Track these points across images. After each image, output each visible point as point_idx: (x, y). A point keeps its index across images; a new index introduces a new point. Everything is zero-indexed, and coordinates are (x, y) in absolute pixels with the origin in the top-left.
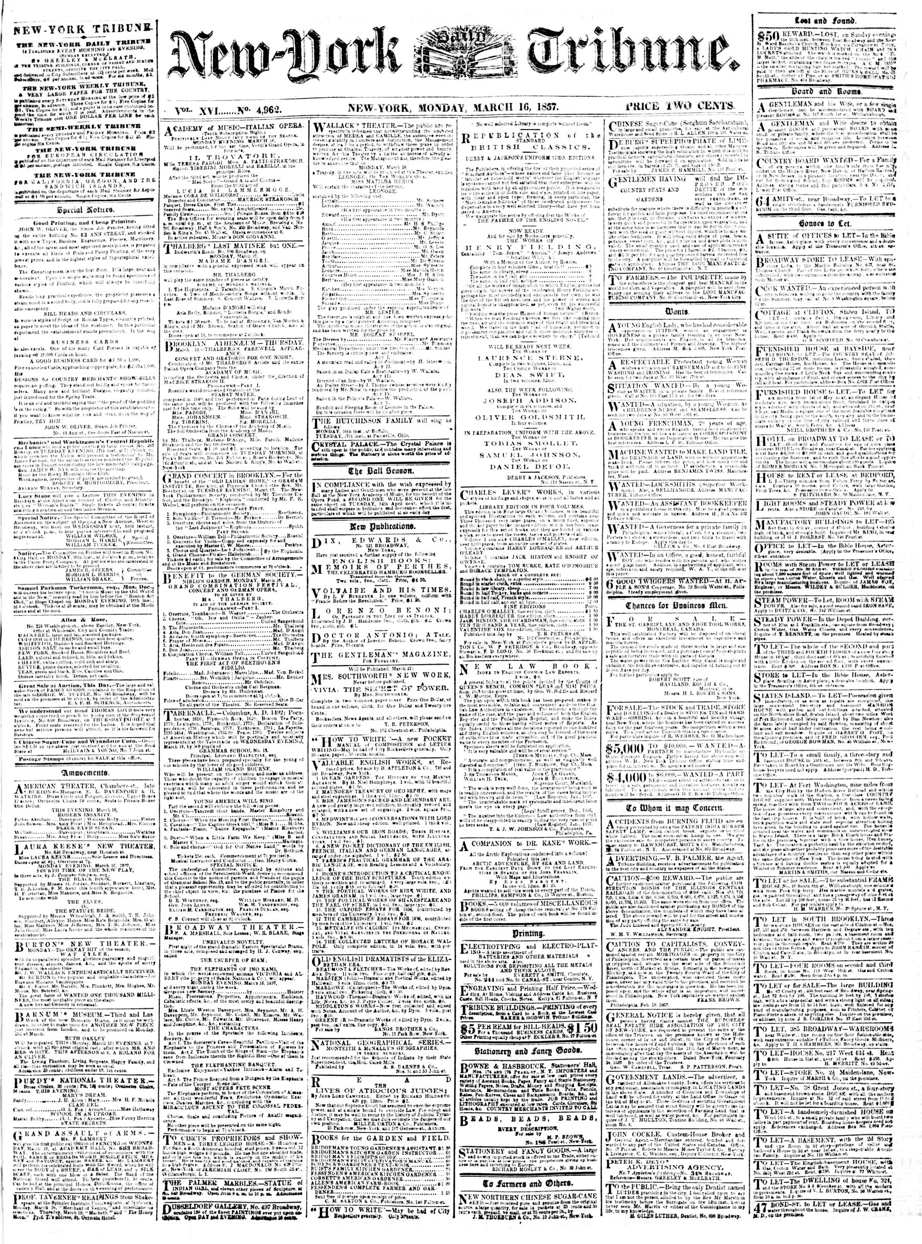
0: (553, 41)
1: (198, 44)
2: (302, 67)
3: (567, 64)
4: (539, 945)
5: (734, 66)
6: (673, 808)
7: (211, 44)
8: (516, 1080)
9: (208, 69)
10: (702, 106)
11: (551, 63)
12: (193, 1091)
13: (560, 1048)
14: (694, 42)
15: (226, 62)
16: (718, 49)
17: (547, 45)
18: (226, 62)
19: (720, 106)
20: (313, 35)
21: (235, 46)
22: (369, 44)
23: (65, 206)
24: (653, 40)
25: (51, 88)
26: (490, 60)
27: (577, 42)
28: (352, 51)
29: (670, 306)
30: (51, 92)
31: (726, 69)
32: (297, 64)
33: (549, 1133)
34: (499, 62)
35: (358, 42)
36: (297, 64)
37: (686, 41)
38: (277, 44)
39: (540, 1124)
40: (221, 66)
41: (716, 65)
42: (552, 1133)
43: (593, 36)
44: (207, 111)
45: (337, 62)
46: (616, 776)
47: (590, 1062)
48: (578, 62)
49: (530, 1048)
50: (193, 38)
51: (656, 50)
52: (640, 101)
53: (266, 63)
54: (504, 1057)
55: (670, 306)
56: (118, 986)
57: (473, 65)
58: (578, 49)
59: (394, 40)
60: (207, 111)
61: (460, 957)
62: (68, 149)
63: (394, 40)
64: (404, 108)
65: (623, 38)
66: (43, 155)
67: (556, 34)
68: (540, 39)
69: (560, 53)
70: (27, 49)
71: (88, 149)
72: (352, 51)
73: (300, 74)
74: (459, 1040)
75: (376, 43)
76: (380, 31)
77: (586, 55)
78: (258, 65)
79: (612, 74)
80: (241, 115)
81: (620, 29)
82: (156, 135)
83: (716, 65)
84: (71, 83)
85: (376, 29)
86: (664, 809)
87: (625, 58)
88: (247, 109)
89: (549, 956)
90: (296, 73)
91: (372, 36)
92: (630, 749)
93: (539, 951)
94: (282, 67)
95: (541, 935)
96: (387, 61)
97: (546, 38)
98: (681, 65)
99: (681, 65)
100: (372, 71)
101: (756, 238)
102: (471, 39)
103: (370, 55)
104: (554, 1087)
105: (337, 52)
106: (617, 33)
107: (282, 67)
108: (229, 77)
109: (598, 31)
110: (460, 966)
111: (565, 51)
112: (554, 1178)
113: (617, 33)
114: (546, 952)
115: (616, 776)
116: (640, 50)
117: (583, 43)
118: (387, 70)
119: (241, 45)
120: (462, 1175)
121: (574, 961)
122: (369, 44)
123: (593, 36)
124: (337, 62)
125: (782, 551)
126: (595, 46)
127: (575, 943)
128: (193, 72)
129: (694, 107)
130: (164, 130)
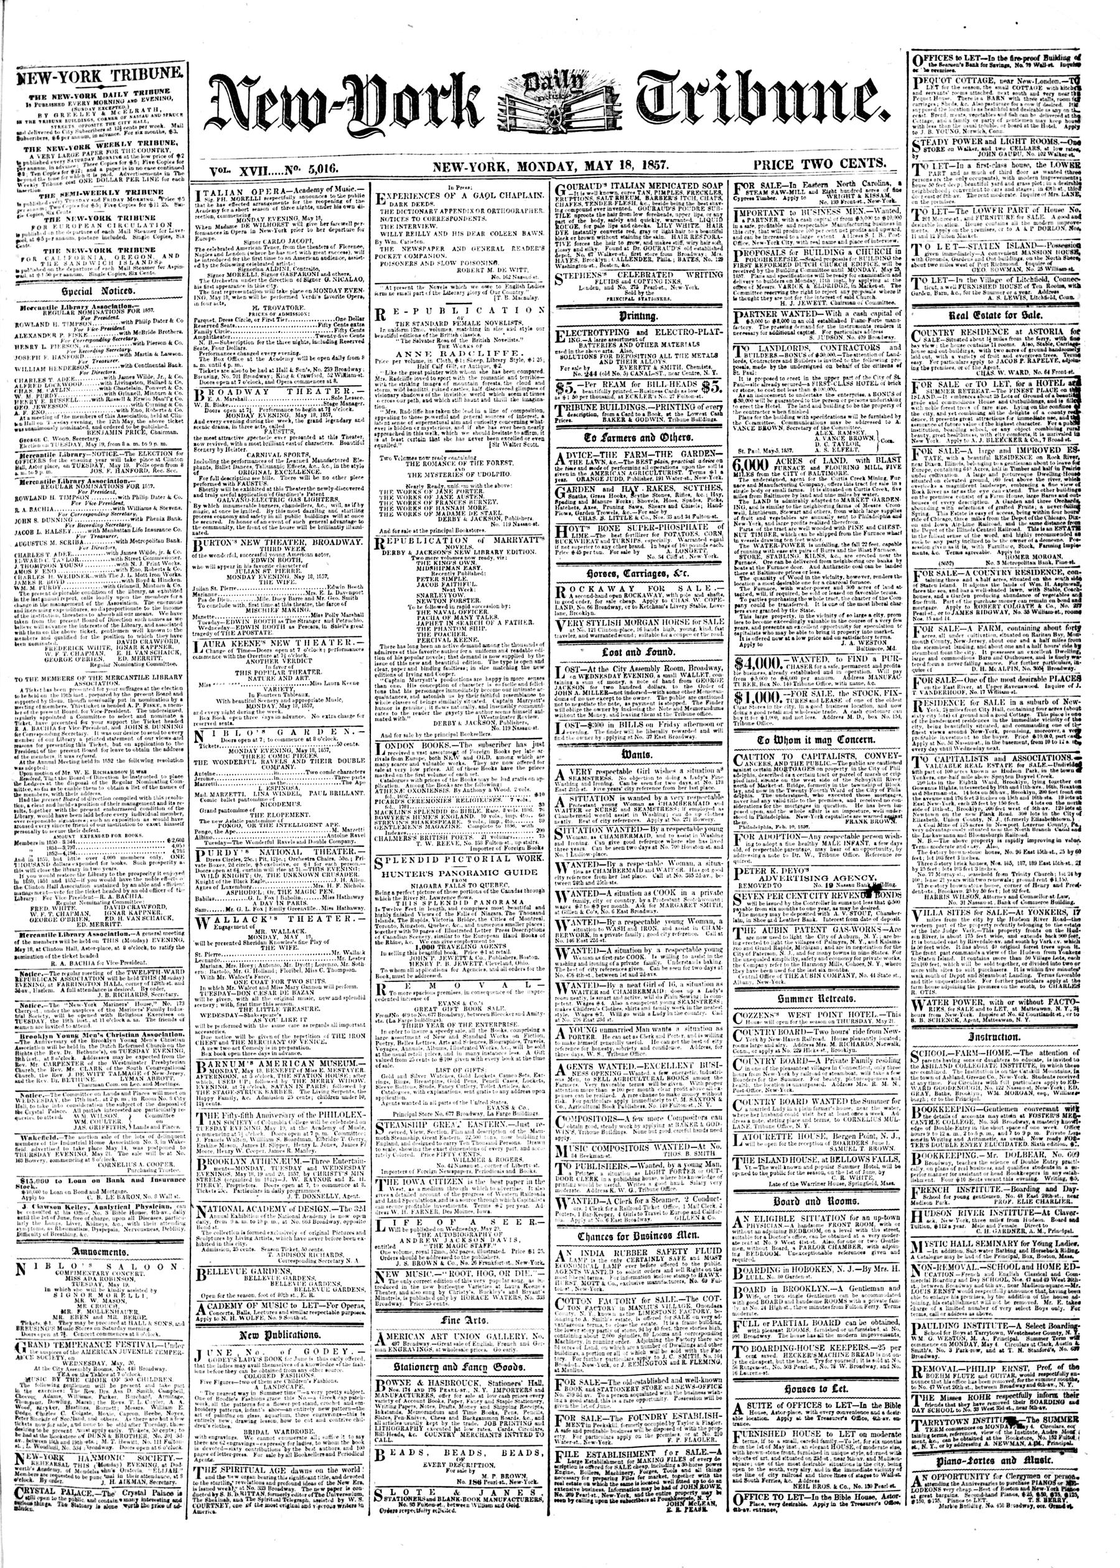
0: (667, 86)
1: (242, 91)
2: (364, 119)
4: (652, 330)
5: (885, 115)
6: (813, 740)
7: (258, 90)
9: (253, 121)
10: (845, 163)
11: (665, 112)
15: (274, 113)
16: (866, 95)
17: (660, 91)
18: (274, 113)
19: (868, 163)
20: (379, 82)
21: (286, 94)
22: (445, 93)
23: (71, 286)
24: (787, 84)
25: (61, 148)
26: (592, 109)
27: (696, 88)
28: (424, 101)
30: (62, 153)
31: (876, 120)
32: (358, 116)
34: (600, 112)
35: (431, 89)
36: (358, 116)
38: (336, 92)
40: (269, 117)
41: (866, 117)
43: (715, 81)
44: (249, 171)
46: (745, 662)
48: (697, 113)
50: (236, 83)
51: (790, 96)
52: (770, 157)
53: (322, 119)
56: (111, 761)
57: (569, 116)
58: (697, 98)
59: (475, 89)
60: (249, 171)
61: (555, 346)
62: (80, 218)
63: (475, 89)
66: (50, 225)
67: (671, 78)
68: (653, 83)
69: (676, 101)
70: (41, 101)
71: (102, 219)
72: (424, 101)
73: (362, 127)
76: (458, 79)
77: (706, 105)
78: (313, 116)
80: (289, 176)
81: (749, 72)
83: (866, 117)
84: (84, 142)
85: (453, 75)
86: (803, 741)
87: (753, 108)
88: (296, 167)
89: (664, 345)
90: (357, 126)
91: (448, 83)
92: (763, 697)
93: (651, 337)
94: (340, 119)
95: (653, 318)
96: (465, 114)
98: (820, 116)
100: (448, 126)
103: (446, 107)
105: (406, 101)
106: (744, 77)
107: (340, 119)
108: (278, 130)
109: (722, 75)
110: (555, 358)
111: (681, 99)
112: (670, 431)
113: (744, 77)
115: (745, 662)
116: (772, 98)
117: (703, 90)
118: (465, 125)
119: (293, 92)
122: (445, 93)
123: (715, 81)
124: (407, 113)
127: (696, 329)
128: (233, 125)
129: (836, 166)
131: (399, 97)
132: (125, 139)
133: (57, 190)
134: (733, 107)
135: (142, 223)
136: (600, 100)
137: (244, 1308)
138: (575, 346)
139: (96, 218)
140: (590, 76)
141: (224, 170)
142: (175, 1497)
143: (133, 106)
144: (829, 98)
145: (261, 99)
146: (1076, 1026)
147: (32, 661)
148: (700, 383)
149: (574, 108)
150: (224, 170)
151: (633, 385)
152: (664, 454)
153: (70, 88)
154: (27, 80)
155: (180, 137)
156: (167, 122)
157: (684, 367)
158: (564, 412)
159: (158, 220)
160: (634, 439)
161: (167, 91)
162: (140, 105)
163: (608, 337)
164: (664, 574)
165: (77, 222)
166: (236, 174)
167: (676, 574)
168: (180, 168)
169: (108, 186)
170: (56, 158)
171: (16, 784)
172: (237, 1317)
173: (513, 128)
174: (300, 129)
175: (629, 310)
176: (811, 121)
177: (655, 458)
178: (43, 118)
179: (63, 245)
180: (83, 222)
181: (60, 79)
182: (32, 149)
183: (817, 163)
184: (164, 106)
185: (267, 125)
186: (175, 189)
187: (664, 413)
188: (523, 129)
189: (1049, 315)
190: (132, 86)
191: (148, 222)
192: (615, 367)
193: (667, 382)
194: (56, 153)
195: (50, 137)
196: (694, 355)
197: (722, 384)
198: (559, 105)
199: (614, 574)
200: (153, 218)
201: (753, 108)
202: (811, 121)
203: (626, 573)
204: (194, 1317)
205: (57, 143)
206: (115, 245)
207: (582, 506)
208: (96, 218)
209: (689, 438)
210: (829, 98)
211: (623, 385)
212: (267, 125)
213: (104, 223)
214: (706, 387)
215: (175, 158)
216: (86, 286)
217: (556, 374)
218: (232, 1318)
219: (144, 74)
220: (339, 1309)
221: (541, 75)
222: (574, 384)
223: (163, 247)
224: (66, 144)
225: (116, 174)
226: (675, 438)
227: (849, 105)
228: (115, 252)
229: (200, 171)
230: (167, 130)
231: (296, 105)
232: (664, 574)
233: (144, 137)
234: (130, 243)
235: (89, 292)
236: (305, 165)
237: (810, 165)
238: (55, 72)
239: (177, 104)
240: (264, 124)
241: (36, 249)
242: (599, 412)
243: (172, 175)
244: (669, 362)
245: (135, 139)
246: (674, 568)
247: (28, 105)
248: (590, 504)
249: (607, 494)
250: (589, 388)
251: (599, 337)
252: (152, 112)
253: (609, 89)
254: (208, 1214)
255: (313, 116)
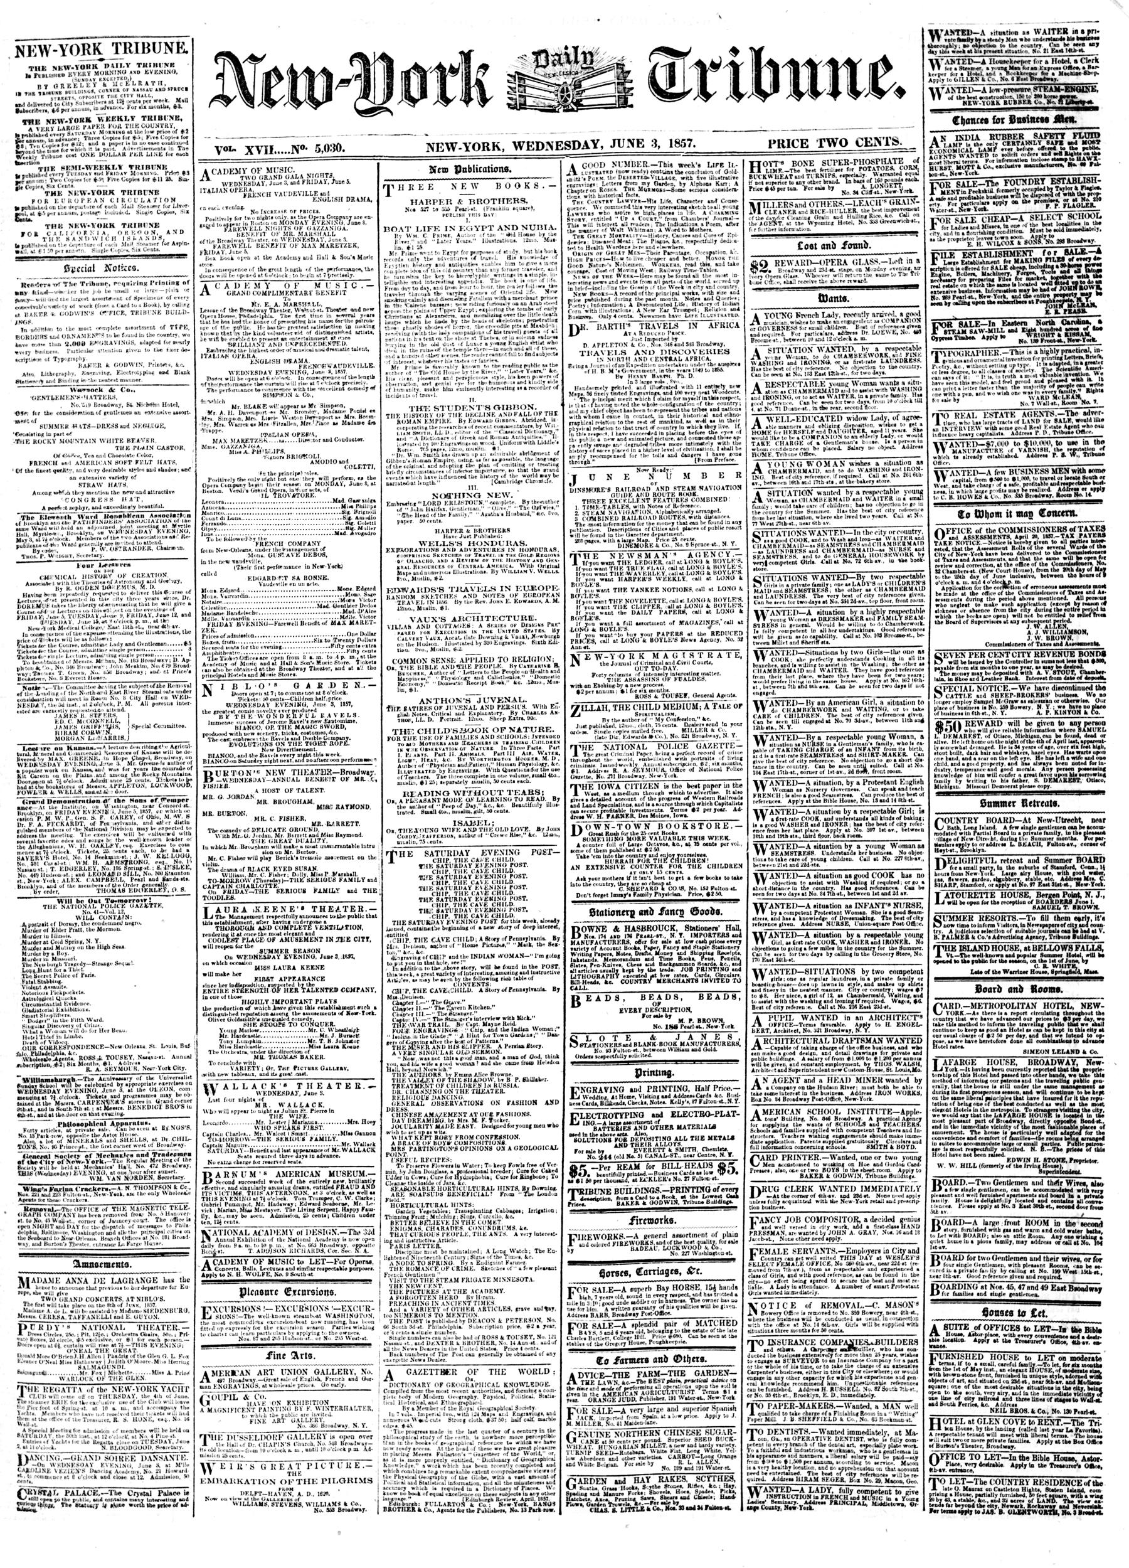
0: (679, 63)
1: (247, 68)
2: (371, 97)
3: (696, 91)
5: (901, 92)
7: (264, 67)
8: (642, 946)
9: (258, 97)
12: (233, 731)
13: (695, 909)
14: (851, 64)
15: (280, 90)
16: (881, 71)
17: (672, 66)
18: (280, 90)
19: (884, 142)
21: (292, 71)
22: (454, 71)
24: (801, 61)
25: (61, 121)
26: (602, 87)
27: (708, 65)
28: (433, 80)
29: (824, 292)
31: (891, 96)
32: (365, 95)
33: (681, 1015)
34: (611, 89)
36: (365, 95)
37: (841, 62)
38: (342, 69)
39: (672, 1003)
40: (275, 94)
41: (880, 93)
42: (686, 1016)
43: (728, 58)
44: (254, 150)
45: (415, 92)
47: (733, 924)
48: (710, 90)
49: (657, 907)
50: (241, 61)
51: (805, 73)
52: (784, 136)
53: (329, 98)
54: (627, 918)
55: (824, 292)
59: (485, 67)
60: (254, 150)
62: (83, 193)
63: (485, 67)
64: (495, 146)
65: (764, 59)
68: (664, 59)
69: (688, 78)
70: (41, 73)
71: (105, 193)
72: (433, 80)
74: (567, 1209)
75: (462, 70)
76: (467, 56)
77: (720, 81)
78: (319, 94)
79: (751, 102)
80: (296, 155)
81: (762, 49)
82: (190, 177)
83: (880, 93)
84: (84, 115)
87: (766, 84)
88: (303, 147)
89: (679, 1127)
90: (364, 105)
91: (457, 61)
94: (347, 97)
96: (475, 93)
97: (669, 59)
98: (835, 93)
99: (835, 93)
100: (457, 105)
101: (928, 1330)
102: (576, 62)
103: (455, 85)
104: (688, 954)
105: (415, 79)
106: (758, 53)
107: (347, 97)
108: (284, 109)
109: (735, 51)
110: (569, 1141)
111: (694, 75)
113: (758, 53)
114: (676, 1122)
116: (785, 75)
117: (715, 66)
118: (474, 104)
119: (299, 69)
120: (571, 1263)
121: (712, 1133)
122: (454, 71)
123: (728, 58)
125: (962, 1462)
126: (730, 69)
128: (239, 103)
130: (199, 174)
131: (407, 75)
132: (129, 113)
133: (58, 163)
134: (746, 84)
135: (146, 198)
136: (611, 76)
137: (250, 1263)
138: (589, 1129)
139: (99, 193)
140: (601, 51)
141: (228, 149)
142: (182, 1496)
143: (136, 78)
144: (844, 74)
145: (268, 75)
146: (1098, 1304)
147: (34, 912)
148: (716, 1164)
149: (585, 84)
150: (228, 149)
151: (648, 1167)
152: (676, 1373)
153: (72, 60)
154: (26, 53)
155: (185, 112)
156: (172, 97)
157: (699, 1149)
158: (577, 1196)
159: (162, 195)
160: (647, 1360)
161: (172, 65)
162: (143, 77)
163: (623, 1120)
164: (676, 1271)
165: (80, 197)
166: (241, 153)
167: (690, 1272)
168: (185, 143)
169: (111, 161)
170: (55, 131)
171: (20, 1315)
172: (243, 1273)
173: (523, 106)
174: (306, 107)
175: (644, 1067)
176: (825, 98)
177: (667, 1378)
178: (43, 90)
179: (65, 220)
180: (86, 197)
181: (60, 51)
182: (31, 122)
183: (832, 142)
184: (169, 80)
185: (272, 103)
186: (177, 164)
187: (678, 1196)
188: (532, 108)
189: (1069, 989)
190: (133, 59)
191: (152, 197)
192: (629, 1150)
193: (682, 1164)
194: (56, 126)
195: (49, 109)
196: (710, 1138)
197: (739, 1166)
198: (569, 81)
199: (626, 1273)
200: (157, 192)
201: (766, 85)
202: (825, 98)
203: (638, 1272)
204: (199, 1273)
205: (58, 116)
206: (118, 220)
207: (593, 1499)
208: (99, 193)
209: (702, 1359)
210: (844, 74)
211: (637, 1167)
212: (272, 103)
213: (107, 198)
214: (722, 1169)
215: (179, 134)
216: (90, 263)
217: (571, 1157)
218: (238, 1274)
219: (147, 48)
220: (347, 1265)
221: (551, 52)
222: (588, 1167)
223: (167, 223)
224: (66, 116)
225: (119, 149)
226: (688, 1359)
227: (864, 81)
228: (118, 226)
229: (204, 149)
230: (171, 105)
231: (302, 82)
232: (676, 1271)
233: (148, 112)
234: (134, 218)
235: (92, 269)
236: (311, 146)
237: (825, 144)
238: (55, 45)
239: (181, 78)
240: (270, 102)
241: (38, 224)
242: (613, 1197)
243: (176, 150)
244: (684, 1144)
245: (138, 114)
246: (688, 1265)
247: (28, 76)
248: (602, 1496)
249: (618, 1486)
250: (603, 1172)
251: (614, 1120)
252: (157, 86)
253: (620, 66)
254: (213, 1239)
255: (319, 94)
